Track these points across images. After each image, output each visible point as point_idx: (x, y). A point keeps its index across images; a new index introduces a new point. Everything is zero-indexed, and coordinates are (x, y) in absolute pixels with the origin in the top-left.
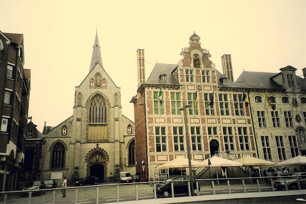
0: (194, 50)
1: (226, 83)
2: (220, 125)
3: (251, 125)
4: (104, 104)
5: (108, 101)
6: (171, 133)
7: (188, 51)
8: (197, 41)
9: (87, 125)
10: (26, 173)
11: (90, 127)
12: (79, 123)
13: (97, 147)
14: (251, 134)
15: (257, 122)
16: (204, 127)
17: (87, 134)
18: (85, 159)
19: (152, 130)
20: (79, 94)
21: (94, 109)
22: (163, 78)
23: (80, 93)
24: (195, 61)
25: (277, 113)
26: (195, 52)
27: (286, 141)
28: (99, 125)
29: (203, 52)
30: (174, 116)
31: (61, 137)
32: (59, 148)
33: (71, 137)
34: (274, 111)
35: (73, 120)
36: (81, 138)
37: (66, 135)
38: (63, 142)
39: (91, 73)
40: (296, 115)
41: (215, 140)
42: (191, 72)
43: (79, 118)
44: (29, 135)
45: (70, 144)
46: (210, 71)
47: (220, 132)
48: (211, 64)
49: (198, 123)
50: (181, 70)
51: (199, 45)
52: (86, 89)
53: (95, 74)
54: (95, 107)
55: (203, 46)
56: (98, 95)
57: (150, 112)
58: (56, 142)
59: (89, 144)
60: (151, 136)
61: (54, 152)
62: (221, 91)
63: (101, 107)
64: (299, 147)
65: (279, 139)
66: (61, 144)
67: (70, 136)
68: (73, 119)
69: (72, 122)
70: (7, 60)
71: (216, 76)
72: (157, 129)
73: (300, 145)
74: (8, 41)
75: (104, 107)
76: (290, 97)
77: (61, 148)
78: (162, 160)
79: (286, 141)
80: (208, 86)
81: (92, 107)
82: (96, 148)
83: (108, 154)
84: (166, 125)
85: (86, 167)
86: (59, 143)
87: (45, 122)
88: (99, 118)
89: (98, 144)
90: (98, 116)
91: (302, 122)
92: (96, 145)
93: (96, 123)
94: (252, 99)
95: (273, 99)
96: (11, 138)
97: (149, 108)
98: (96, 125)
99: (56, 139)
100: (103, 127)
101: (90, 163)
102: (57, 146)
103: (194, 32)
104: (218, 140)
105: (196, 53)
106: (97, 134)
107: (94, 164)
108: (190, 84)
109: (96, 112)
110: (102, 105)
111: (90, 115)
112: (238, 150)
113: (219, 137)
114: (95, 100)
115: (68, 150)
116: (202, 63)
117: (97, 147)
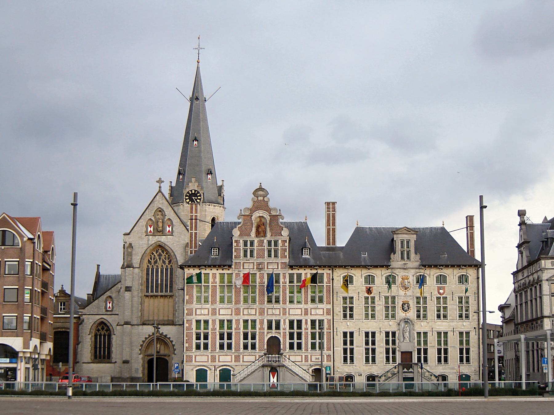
0: (258, 211)
1: (307, 254)
2: (284, 317)
3: (330, 317)
4: (170, 262)
5: (175, 257)
6: (215, 327)
7: (248, 214)
8: (264, 197)
9: (141, 297)
10: (61, 364)
11: (147, 300)
12: (127, 294)
15: (340, 313)
16: (262, 320)
17: (142, 311)
18: (140, 350)
21: (152, 269)
22: (214, 252)
23: (130, 244)
24: (258, 227)
25: (373, 298)
26: (259, 214)
27: (380, 339)
28: (161, 296)
29: (272, 213)
31: (104, 314)
32: (103, 330)
33: (118, 315)
34: (370, 296)
35: (121, 288)
36: (131, 318)
37: (112, 311)
39: (147, 210)
40: (403, 302)
41: (275, 336)
42: (252, 243)
43: (129, 285)
44: (61, 308)
45: (117, 325)
46: (280, 241)
47: (285, 326)
49: (254, 315)
50: (236, 241)
51: (267, 202)
52: (140, 237)
53: (155, 210)
55: (271, 205)
56: (161, 247)
58: (98, 322)
60: (189, 331)
61: (96, 336)
62: (292, 270)
64: (398, 347)
65: (370, 337)
67: (117, 313)
68: (122, 286)
69: (120, 290)
70: (25, 259)
71: (287, 248)
73: (400, 344)
74: (25, 237)
76: (398, 276)
77: (105, 330)
79: (380, 339)
80: (274, 263)
83: (173, 343)
84: (210, 318)
85: (141, 361)
86: (102, 323)
87: (98, 266)
88: (162, 284)
90: (159, 282)
91: (411, 311)
93: (156, 294)
94: (338, 279)
95: (370, 279)
96: (34, 335)
97: (188, 296)
98: (157, 296)
99: (98, 317)
100: (166, 300)
101: (148, 356)
102: (100, 328)
103: (261, 184)
104: (279, 337)
105: (261, 215)
106: (157, 311)
108: (248, 262)
109: (157, 276)
111: (147, 279)
112: (307, 350)
113: (282, 334)
114: (155, 256)
115: (115, 335)
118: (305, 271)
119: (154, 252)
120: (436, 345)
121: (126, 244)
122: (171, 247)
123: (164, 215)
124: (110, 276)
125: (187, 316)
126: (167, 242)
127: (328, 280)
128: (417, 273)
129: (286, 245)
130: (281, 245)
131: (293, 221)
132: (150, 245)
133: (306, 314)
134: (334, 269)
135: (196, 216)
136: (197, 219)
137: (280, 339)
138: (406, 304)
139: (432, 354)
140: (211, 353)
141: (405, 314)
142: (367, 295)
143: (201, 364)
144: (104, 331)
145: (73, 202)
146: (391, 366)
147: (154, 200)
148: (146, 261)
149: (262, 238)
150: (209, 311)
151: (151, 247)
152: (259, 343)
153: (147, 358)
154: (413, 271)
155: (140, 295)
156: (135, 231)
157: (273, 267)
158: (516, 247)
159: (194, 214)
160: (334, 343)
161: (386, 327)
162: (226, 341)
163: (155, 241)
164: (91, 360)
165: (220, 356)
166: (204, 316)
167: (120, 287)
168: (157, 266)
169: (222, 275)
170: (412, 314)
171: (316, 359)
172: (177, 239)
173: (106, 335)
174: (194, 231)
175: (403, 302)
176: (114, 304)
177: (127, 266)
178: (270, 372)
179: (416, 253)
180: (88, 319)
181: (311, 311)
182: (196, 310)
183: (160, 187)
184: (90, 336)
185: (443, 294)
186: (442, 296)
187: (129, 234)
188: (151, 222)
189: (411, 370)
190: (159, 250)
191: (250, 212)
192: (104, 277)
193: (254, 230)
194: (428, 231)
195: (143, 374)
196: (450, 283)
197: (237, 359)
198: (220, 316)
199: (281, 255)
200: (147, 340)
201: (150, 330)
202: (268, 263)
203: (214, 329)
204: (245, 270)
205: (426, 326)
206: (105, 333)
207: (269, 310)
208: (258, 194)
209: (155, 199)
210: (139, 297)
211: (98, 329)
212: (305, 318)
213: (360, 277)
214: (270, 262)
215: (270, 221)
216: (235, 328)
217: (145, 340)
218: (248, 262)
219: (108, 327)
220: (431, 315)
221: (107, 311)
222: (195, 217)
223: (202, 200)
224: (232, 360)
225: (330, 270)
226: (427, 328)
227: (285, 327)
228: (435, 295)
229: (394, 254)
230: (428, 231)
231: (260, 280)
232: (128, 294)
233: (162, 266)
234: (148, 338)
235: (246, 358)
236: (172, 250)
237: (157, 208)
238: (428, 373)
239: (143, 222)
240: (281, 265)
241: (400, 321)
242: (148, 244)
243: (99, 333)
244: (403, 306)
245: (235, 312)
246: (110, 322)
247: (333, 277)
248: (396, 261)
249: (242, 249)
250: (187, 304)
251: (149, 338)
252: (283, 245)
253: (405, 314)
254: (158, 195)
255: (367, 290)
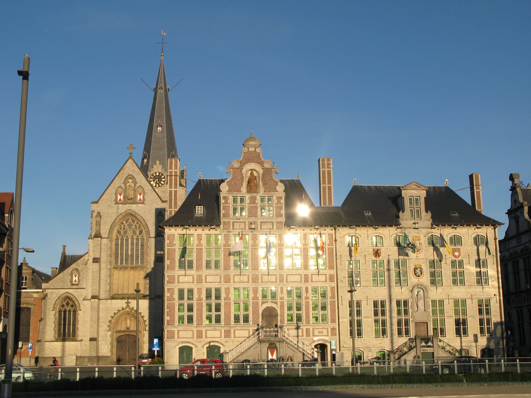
0: (249, 164)
3: (334, 284)
4: (141, 232)
9: (110, 269)
11: (116, 272)
12: (96, 265)
13: (128, 305)
14: (333, 297)
17: (110, 284)
18: (109, 326)
19: (173, 293)
20: (97, 216)
23: (99, 213)
30: (208, 272)
31: (70, 288)
32: (68, 306)
35: (88, 260)
37: (77, 285)
38: (74, 297)
39: (117, 177)
42: (242, 200)
43: (96, 257)
45: (84, 300)
46: (275, 198)
48: (277, 185)
49: (246, 282)
50: (225, 198)
52: (109, 206)
53: (125, 177)
54: (125, 238)
56: (132, 215)
57: (171, 267)
58: (62, 297)
59: (114, 301)
61: (60, 311)
63: (135, 237)
66: (70, 299)
67: (84, 287)
68: (89, 258)
71: (283, 205)
72: (181, 292)
73: (414, 314)
75: (140, 237)
77: (70, 306)
78: (184, 337)
81: (120, 237)
82: (125, 308)
85: (109, 339)
86: (68, 297)
89: (130, 301)
90: (130, 253)
91: (424, 276)
92: (126, 303)
94: (341, 240)
97: (169, 261)
102: (65, 304)
104: (275, 307)
105: (253, 168)
107: (123, 334)
108: (238, 221)
110: (138, 234)
111: (117, 249)
113: (279, 304)
114: (124, 226)
115: (81, 310)
116: (261, 184)
117: (128, 305)
118: (303, 231)
119: (123, 222)
120: (454, 315)
121: (93, 213)
122: (142, 216)
123: (135, 183)
124: (76, 256)
125: (168, 284)
126: (138, 210)
127: (330, 242)
128: (429, 233)
129: (281, 202)
130: (276, 202)
131: (284, 179)
132: (119, 214)
133: (306, 280)
134: (337, 229)
135: (176, 172)
136: (177, 176)
137: (277, 309)
138: (419, 269)
139: (450, 326)
140: (197, 327)
141: (418, 280)
142: (374, 258)
143: (185, 340)
144: (69, 306)
145: (21, 69)
146: (404, 339)
147: (124, 167)
148: (115, 231)
149: (255, 194)
150: (193, 278)
151: (121, 216)
152: (253, 315)
153: (117, 335)
154: (424, 231)
155: (108, 267)
156: (104, 199)
157: (268, 226)
158: (506, 213)
159: (173, 170)
160: (340, 314)
161: (398, 295)
162: (214, 313)
163: (125, 209)
164: (54, 338)
165: (208, 332)
166: (187, 284)
167: (87, 258)
168: (127, 237)
169: (209, 236)
170: (425, 279)
171: (319, 332)
172: (149, 208)
173: (71, 311)
174: (173, 189)
175: (415, 266)
176: (80, 278)
177: (94, 236)
178: (268, 348)
179: (427, 212)
180: (52, 293)
181: (312, 278)
182: (178, 276)
183: (131, 153)
184: (54, 312)
185: (459, 256)
186: (457, 259)
187: (96, 202)
188: (121, 190)
189: (430, 344)
190: (129, 219)
191: (240, 164)
192: (69, 258)
193: (245, 184)
194: (432, 190)
195: (112, 353)
196: (465, 244)
197: (227, 334)
198: (207, 284)
199: (276, 213)
200: (116, 316)
201: (120, 304)
202: (261, 222)
203: (200, 299)
204: (235, 230)
205: (442, 294)
206: (70, 309)
207: (263, 276)
208: (249, 144)
209: (125, 166)
210: (107, 269)
211: (63, 304)
212: (305, 285)
213: (366, 238)
214: (264, 221)
215: (263, 175)
216: (224, 298)
217: (114, 315)
218: (238, 221)
219: (73, 302)
220: (447, 280)
221: (73, 285)
222: (175, 173)
223: (166, 182)
224: (221, 335)
225: (332, 230)
226: (442, 295)
227: (283, 296)
228: (449, 258)
229: (403, 212)
230: (432, 190)
231: (253, 242)
232: (95, 266)
233: (132, 236)
234: (117, 313)
235: (238, 333)
236: (143, 218)
237: (127, 175)
238: (449, 347)
239: (112, 190)
240: (276, 224)
241: (413, 288)
242: (118, 213)
243: (63, 309)
244: (415, 271)
245: (224, 278)
246: (76, 297)
247: (335, 238)
248: (405, 218)
249: (231, 206)
250: (168, 270)
251: (119, 314)
252: (279, 202)
253: (418, 280)
254: (128, 161)
255: (374, 252)
